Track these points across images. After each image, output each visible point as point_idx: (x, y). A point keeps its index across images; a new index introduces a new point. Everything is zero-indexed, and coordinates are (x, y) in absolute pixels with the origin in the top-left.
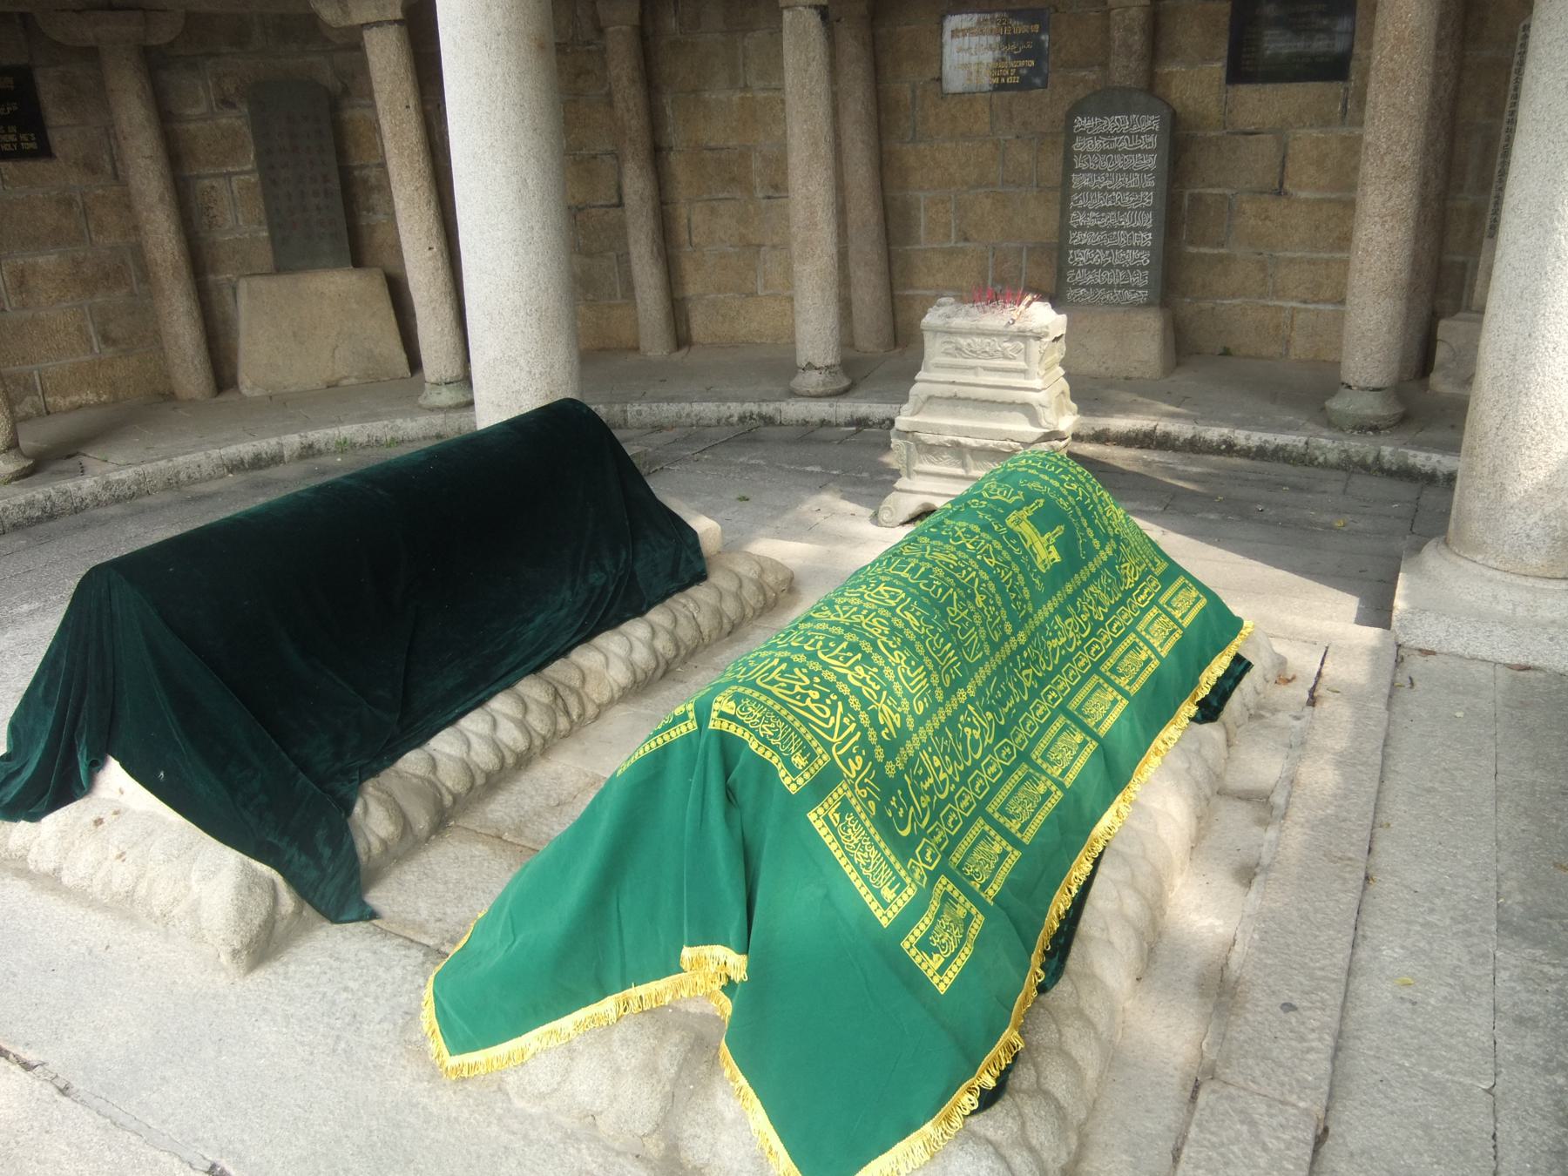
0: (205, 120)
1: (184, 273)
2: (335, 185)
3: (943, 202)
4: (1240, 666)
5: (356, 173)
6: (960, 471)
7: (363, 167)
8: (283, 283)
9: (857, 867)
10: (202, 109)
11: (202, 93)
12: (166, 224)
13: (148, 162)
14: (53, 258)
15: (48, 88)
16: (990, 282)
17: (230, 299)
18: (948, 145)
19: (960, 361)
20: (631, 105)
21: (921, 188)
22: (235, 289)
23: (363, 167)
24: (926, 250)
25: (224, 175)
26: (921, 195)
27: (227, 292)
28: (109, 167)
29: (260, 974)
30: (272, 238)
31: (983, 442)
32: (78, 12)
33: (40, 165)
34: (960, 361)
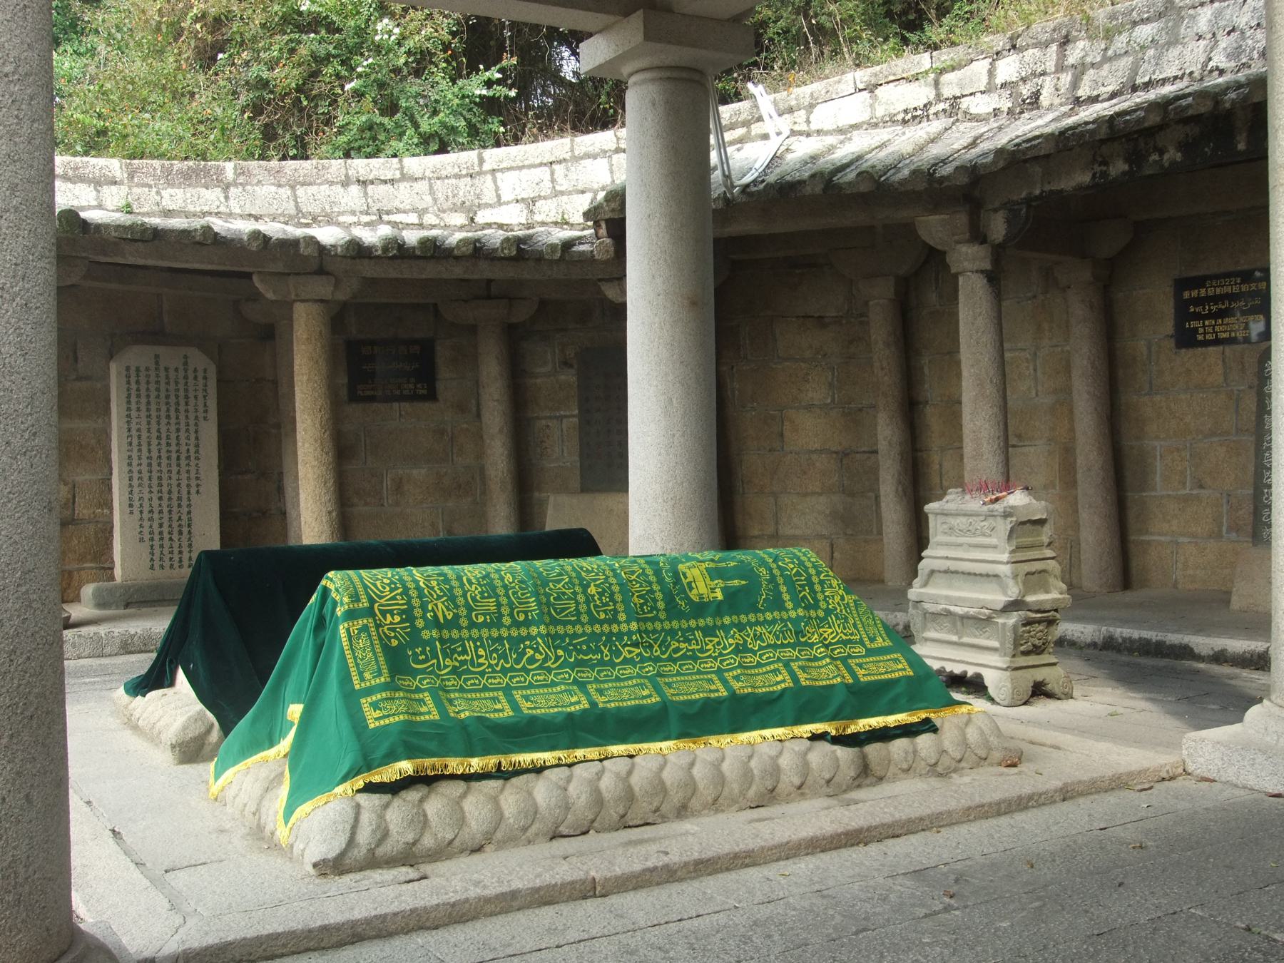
1: (509, 487)
3: (1178, 450)
4: (927, 726)
6: (955, 638)
8: (587, 497)
9: (355, 658)
12: (501, 450)
14: (423, 471)
15: (443, 353)
16: (1224, 529)
18: (1183, 396)
19: (953, 539)
20: (885, 364)
21: (1157, 438)
24: (1162, 497)
25: (556, 418)
26: (1156, 443)
28: (474, 409)
29: (186, 767)
31: (966, 609)
32: (466, 301)
33: (427, 406)
34: (953, 539)
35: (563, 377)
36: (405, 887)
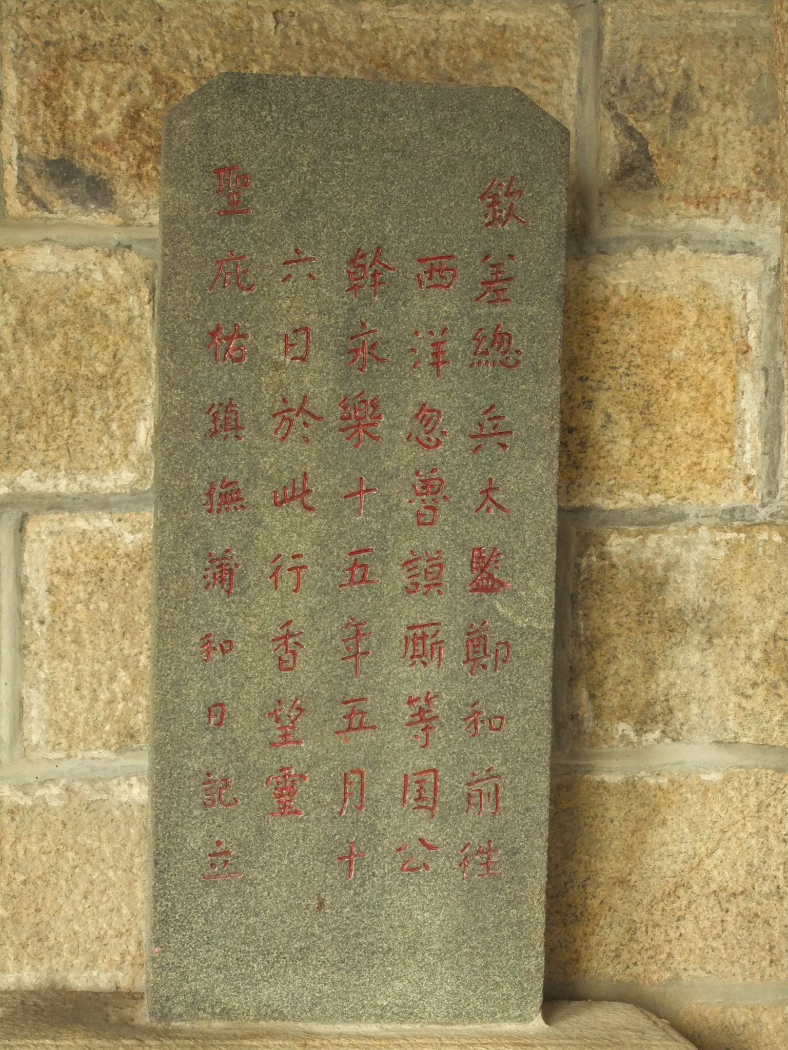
2: (528, 606)
5: (616, 544)
23: (653, 520)
35: (43, 259)
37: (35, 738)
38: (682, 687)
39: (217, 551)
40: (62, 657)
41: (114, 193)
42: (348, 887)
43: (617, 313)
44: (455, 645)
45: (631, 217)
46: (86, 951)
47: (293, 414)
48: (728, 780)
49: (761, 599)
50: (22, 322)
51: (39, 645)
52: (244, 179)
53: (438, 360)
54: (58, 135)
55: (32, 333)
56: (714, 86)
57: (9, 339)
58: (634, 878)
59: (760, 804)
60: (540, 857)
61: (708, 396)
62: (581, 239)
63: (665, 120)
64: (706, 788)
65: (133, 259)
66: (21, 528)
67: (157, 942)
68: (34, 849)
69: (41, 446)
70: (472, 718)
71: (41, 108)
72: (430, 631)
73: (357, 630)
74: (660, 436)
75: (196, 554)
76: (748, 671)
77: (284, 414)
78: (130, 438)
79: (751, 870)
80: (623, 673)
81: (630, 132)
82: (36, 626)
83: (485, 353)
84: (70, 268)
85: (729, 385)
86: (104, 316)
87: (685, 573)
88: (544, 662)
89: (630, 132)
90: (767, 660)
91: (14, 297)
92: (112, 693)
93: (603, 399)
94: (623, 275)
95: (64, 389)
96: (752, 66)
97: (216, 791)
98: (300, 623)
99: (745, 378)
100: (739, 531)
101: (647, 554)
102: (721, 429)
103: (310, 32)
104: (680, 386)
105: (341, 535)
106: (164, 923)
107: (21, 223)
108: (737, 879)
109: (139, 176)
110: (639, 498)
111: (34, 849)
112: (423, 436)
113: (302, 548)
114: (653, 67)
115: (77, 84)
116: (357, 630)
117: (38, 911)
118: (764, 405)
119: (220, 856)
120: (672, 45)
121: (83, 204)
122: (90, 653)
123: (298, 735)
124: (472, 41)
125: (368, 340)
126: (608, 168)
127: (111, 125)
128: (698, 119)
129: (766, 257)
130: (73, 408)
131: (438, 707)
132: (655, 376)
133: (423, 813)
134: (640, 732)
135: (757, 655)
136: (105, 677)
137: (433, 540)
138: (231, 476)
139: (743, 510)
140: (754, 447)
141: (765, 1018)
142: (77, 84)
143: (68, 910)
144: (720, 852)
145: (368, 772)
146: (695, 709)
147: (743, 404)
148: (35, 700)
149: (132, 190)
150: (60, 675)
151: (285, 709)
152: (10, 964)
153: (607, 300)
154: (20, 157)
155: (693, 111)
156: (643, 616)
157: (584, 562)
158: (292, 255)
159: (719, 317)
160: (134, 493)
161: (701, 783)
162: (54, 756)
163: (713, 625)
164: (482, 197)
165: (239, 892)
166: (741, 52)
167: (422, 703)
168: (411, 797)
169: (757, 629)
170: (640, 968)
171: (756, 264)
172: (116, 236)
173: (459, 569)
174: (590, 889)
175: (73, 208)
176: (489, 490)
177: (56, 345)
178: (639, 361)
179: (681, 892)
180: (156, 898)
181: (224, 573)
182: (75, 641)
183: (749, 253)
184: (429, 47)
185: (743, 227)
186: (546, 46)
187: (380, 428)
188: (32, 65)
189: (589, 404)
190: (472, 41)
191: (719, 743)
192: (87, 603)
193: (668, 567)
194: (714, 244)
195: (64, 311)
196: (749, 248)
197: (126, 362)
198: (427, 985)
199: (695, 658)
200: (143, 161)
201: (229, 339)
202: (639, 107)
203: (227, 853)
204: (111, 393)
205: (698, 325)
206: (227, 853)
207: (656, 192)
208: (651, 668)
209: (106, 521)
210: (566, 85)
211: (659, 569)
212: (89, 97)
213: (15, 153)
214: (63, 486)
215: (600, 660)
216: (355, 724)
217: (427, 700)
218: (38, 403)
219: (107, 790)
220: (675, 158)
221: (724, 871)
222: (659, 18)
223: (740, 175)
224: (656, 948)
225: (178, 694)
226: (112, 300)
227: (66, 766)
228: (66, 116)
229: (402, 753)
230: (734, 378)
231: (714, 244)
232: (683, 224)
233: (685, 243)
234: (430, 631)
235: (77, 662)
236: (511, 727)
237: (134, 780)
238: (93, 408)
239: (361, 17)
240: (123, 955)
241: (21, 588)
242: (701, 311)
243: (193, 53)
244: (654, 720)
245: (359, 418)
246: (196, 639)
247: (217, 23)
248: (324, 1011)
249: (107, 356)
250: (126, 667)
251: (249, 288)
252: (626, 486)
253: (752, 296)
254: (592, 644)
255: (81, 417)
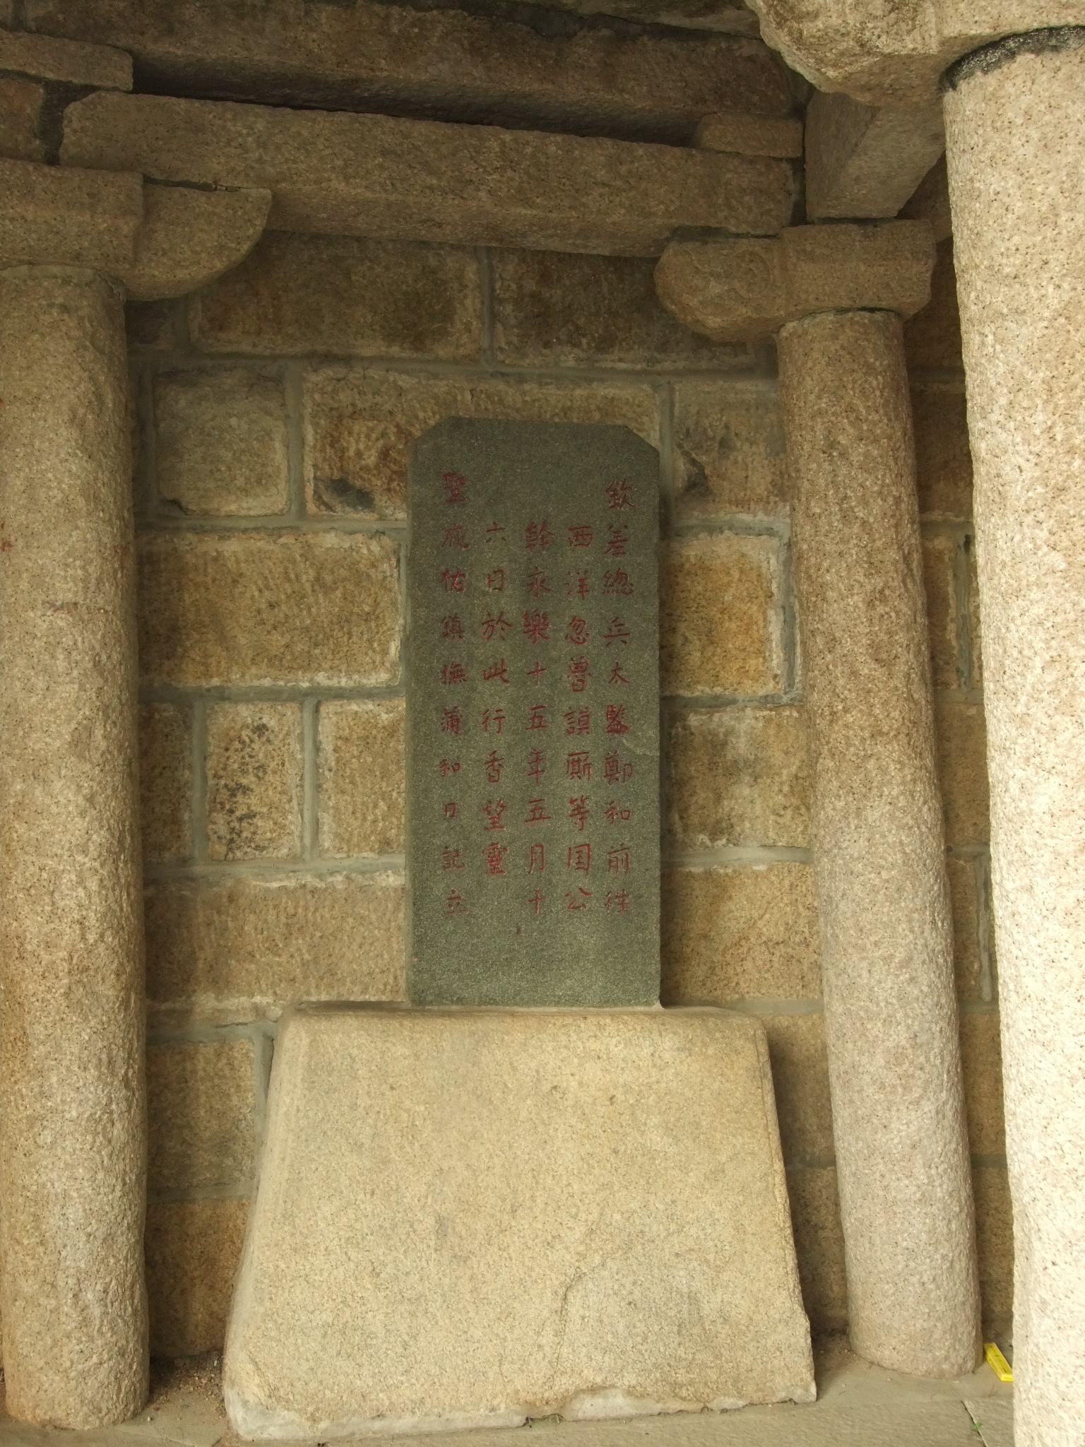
0: (276, 533)
1: (109, 989)
2: (643, 741)
5: (694, 720)
7: (717, 704)
10: (274, 500)
11: (279, 455)
13: (62, 620)
17: (250, 1074)
22: (270, 1044)
23: (717, 704)
25: (298, 697)
27: (248, 1048)
30: (418, 895)
35: (330, 540)
36: (97, 83)
37: (327, 845)
38: (738, 810)
39: (449, 707)
40: (343, 792)
41: (373, 499)
42: (535, 919)
43: (689, 573)
44: (598, 766)
45: (696, 513)
46: (361, 983)
47: (494, 623)
48: (770, 869)
49: (786, 753)
50: (317, 579)
51: (328, 785)
52: (462, 480)
53: (583, 589)
54: (339, 465)
55: (323, 586)
56: (744, 433)
57: (309, 590)
58: (713, 933)
59: (791, 885)
60: (656, 899)
61: (748, 624)
62: (668, 527)
63: (715, 454)
64: (756, 875)
65: (386, 540)
66: (317, 711)
67: (416, 955)
68: (327, 916)
69: (330, 657)
70: (610, 812)
71: (328, 449)
72: (582, 757)
73: (537, 757)
74: (719, 650)
75: (436, 709)
76: (780, 799)
77: (488, 622)
78: (385, 652)
79: (788, 927)
80: (701, 802)
81: (693, 462)
82: (327, 773)
83: (612, 585)
84: (347, 545)
85: (761, 618)
86: (368, 576)
87: (739, 737)
88: (654, 776)
89: (693, 462)
90: (792, 792)
91: (312, 564)
92: (376, 815)
93: (682, 627)
94: (693, 550)
95: (344, 621)
96: (767, 420)
97: (451, 858)
98: (502, 752)
99: (771, 613)
100: (771, 710)
101: (713, 726)
102: (756, 646)
103: (493, 402)
104: (730, 619)
105: (526, 697)
106: (421, 943)
107: (317, 518)
108: (778, 933)
109: (389, 490)
110: (707, 690)
111: (327, 916)
112: (575, 636)
113: (502, 705)
114: (706, 422)
115: (350, 433)
116: (537, 757)
117: (330, 956)
118: (783, 629)
119: (453, 899)
120: (717, 408)
121: (354, 507)
122: (361, 789)
123: (502, 823)
124: (593, 407)
125: (540, 577)
126: (680, 484)
127: (371, 459)
128: (735, 453)
129: (781, 538)
130: (350, 634)
131: (589, 805)
132: (714, 612)
133: (581, 872)
134: (713, 840)
135: (786, 789)
136: (371, 805)
137: (583, 700)
138: (458, 661)
139: (773, 696)
140: (778, 657)
141: (800, 1022)
142: (350, 433)
143: (349, 955)
144: (767, 916)
145: (546, 846)
146: (747, 825)
147: (770, 629)
148: (327, 819)
149: (385, 498)
150: (342, 804)
151: (494, 806)
152: (312, 990)
153: (683, 565)
154: (315, 478)
155: (732, 448)
156: (712, 766)
157: (674, 732)
158: (492, 527)
159: (753, 575)
160: (388, 687)
161: (753, 872)
162: (338, 856)
163: (757, 770)
164: (607, 491)
165: (467, 922)
166: (760, 412)
167: (579, 802)
168: (573, 863)
169: (785, 772)
170: (719, 992)
171: (775, 542)
172: (376, 526)
173: (599, 718)
174: (685, 941)
175: (347, 509)
176: (617, 669)
177: (338, 593)
178: (704, 603)
179: (743, 942)
180: (415, 927)
181: (454, 721)
182: (351, 782)
183: (770, 535)
184: (566, 411)
185: (766, 518)
186: (638, 410)
187: (548, 632)
188: (322, 422)
189: (674, 630)
190: (593, 407)
191: (764, 846)
192: (359, 758)
193: (727, 734)
194: (748, 530)
195: (343, 573)
196: (770, 532)
197: (382, 604)
198: (587, 982)
199: (746, 791)
200: (391, 480)
201: (454, 577)
202: (698, 446)
203: (459, 897)
204: (373, 624)
205: (740, 580)
206: (459, 897)
207: (711, 498)
208: (718, 799)
209: (370, 706)
210: (652, 433)
211: (721, 735)
212: (357, 441)
213: (312, 476)
214: (344, 682)
215: (686, 794)
216: (537, 816)
217: (582, 801)
218: (328, 630)
219: (372, 879)
220: (721, 477)
221: (770, 927)
222: (709, 393)
223: (763, 487)
224: (729, 979)
225: (426, 798)
226: (373, 566)
227: (346, 863)
228: (343, 452)
229: (567, 833)
230: (764, 613)
231: (748, 530)
232: (728, 517)
233: (730, 529)
234: (582, 757)
235: (353, 796)
236: (635, 818)
237: (390, 872)
238: (362, 633)
239: (524, 393)
240: (385, 985)
241: (317, 748)
242: (742, 571)
243: (421, 415)
244: (722, 832)
245: (535, 625)
246: (437, 763)
247: (436, 397)
248: (522, 999)
249: (370, 601)
250: (383, 799)
251: (466, 546)
252: (698, 682)
253: (773, 561)
254: (681, 783)
255: (355, 639)
